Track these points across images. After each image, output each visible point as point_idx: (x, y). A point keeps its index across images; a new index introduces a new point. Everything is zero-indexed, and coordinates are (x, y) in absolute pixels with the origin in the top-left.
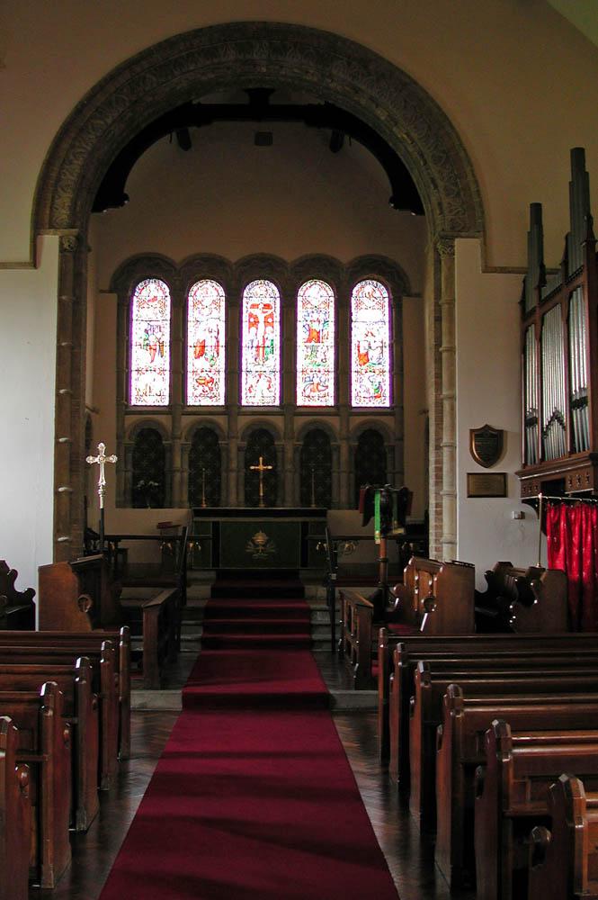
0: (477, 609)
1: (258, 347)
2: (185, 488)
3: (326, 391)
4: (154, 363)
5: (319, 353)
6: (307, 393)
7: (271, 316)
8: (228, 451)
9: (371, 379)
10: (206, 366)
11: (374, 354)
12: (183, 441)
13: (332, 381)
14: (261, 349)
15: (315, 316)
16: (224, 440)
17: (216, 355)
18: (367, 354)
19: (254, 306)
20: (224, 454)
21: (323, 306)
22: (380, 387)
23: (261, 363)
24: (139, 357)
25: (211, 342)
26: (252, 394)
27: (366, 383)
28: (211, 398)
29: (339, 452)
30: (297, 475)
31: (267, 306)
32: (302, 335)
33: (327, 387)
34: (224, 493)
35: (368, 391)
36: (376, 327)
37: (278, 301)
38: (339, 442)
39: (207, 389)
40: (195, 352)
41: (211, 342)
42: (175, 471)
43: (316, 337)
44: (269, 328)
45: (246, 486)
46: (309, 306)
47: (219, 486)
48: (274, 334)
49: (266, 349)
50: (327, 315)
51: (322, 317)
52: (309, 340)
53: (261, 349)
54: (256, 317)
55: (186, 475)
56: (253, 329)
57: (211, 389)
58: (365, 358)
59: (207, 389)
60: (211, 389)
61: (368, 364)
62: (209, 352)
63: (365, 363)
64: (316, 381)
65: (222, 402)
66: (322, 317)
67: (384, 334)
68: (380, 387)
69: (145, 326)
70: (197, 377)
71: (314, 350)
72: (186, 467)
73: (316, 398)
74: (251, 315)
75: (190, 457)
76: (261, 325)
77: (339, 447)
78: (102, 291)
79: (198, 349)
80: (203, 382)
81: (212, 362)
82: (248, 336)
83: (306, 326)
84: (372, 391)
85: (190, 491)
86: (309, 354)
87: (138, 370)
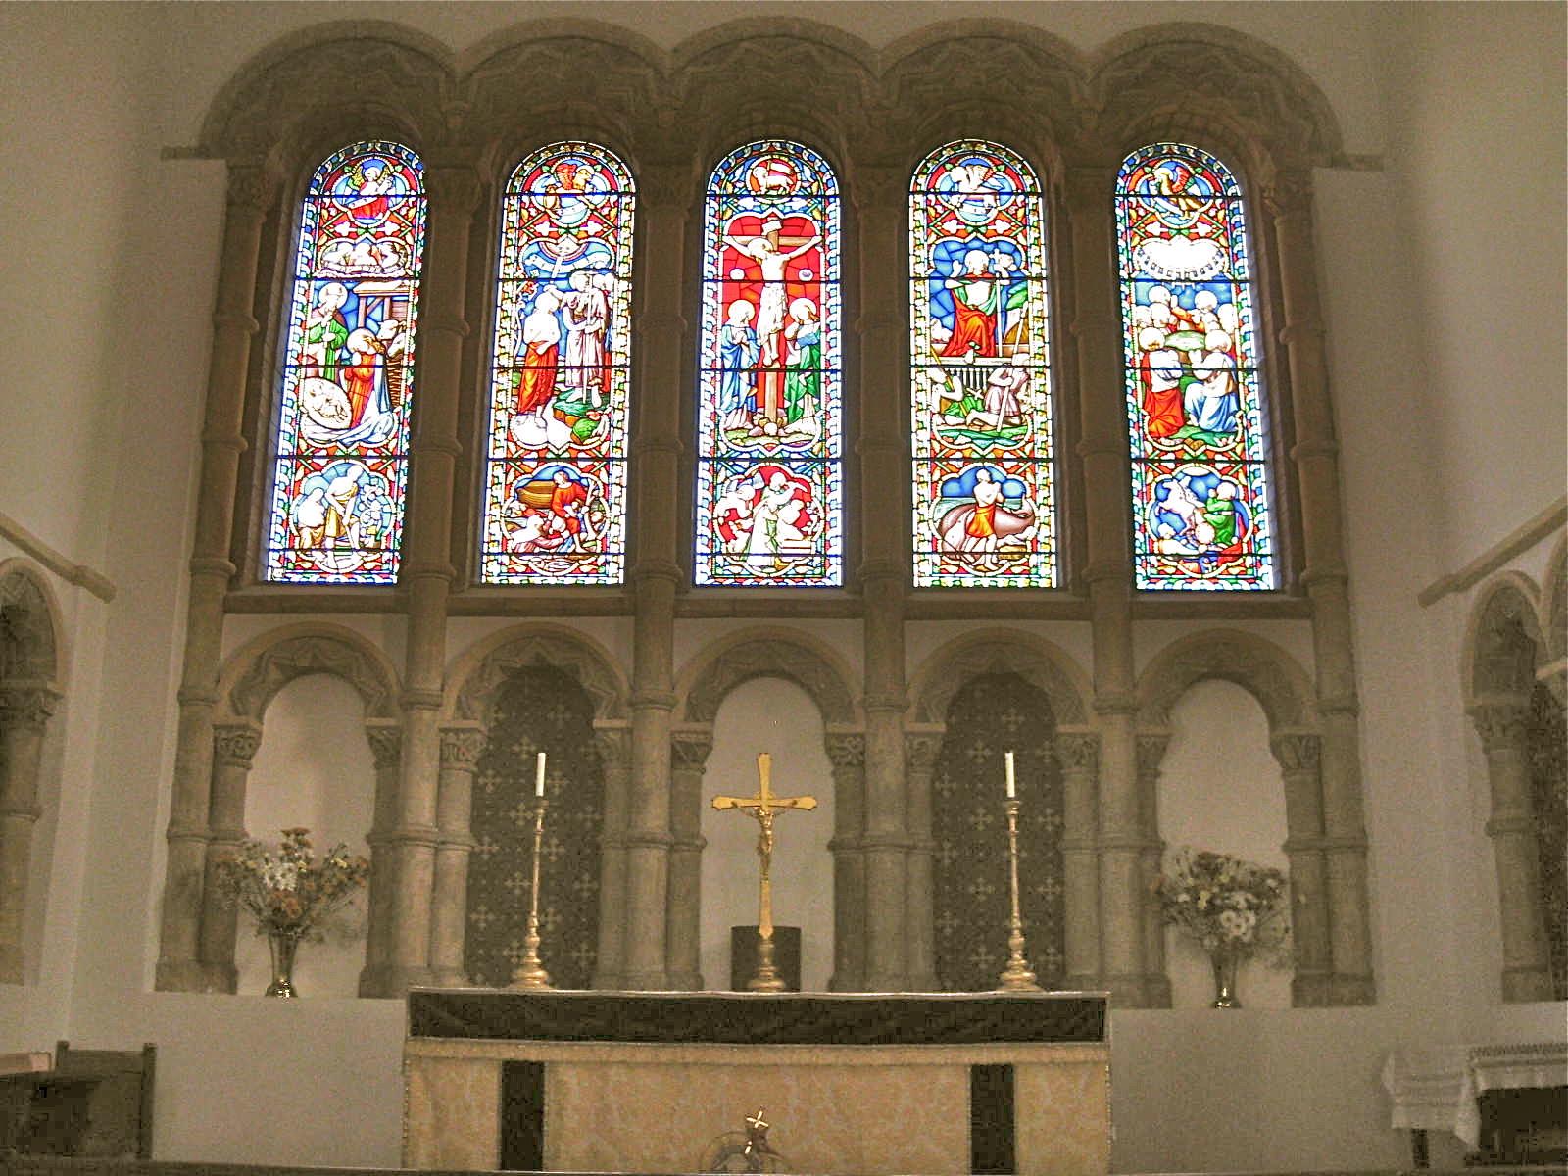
0: (766, 932)
1: (758, 370)
2: (452, 914)
3: (1030, 533)
4: (362, 431)
5: (994, 393)
6: (955, 536)
7: (811, 259)
8: (631, 762)
9: (1200, 486)
10: (559, 435)
11: (1206, 397)
12: (448, 715)
13: (1047, 495)
14: (771, 377)
15: (976, 261)
16: (614, 714)
17: (596, 401)
18: (1178, 395)
19: (743, 227)
20: (614, 772)
21: (1001, 227)
22: (1235, 517)
23: (771, 429)
24: (313, 405)
25: (580, 352)
26: (738, 545)
27: (1180, 502)
28: (572, 557)
29: (1096, 767)
30: (920, 865)
31: (794, 227)
32: (927, 331)
33: (1029, 518)
34: (609, 937)
35: (1186, 533)
36: (1205, 299)
37: (834, 210)
38: (1093, 725)
39: (558, 524)
40: (519, 389)
41: (580, 352)
42: (405, 839)
43: (973, 336)
44: (801, 308)
45: (471, 907)
46: (951, 226)
47: (474, 894)
48: (820, 325)
49: (792, 379)
50: (1021, 257)
51: (1003, 263)
52: (955, 347)
53: (771, 377)
54: (754, 263)
55: (456, 858)
56: (741, 309)
57: (574, 526)
58: (1172, 409)
59: (558, 524)
60: (574, 526)
61: (1182, 434)
62: (573, 389)
63: (1171, 431)
64: (986, 493)
65: (614, 573)
66: (1003, 263)
67: (1231, 324)
68: (1235, 517)
69: (334, 296)
70: (523, 481)
71: (977, 384)
72: (459, 824)
73: (988, 561)
74: (734, 258)
75: (477, 789)
76: (772, 296)
77: (1090, 753)
78: (175, 154)
79: (530, 378)
80: (545, 497)
81: (582, 426)
82: (722, 325)
83: (945, 297)
84: (1205, 534)
85: (471, 928)
86: (958, 395)
87: (297, 456)
